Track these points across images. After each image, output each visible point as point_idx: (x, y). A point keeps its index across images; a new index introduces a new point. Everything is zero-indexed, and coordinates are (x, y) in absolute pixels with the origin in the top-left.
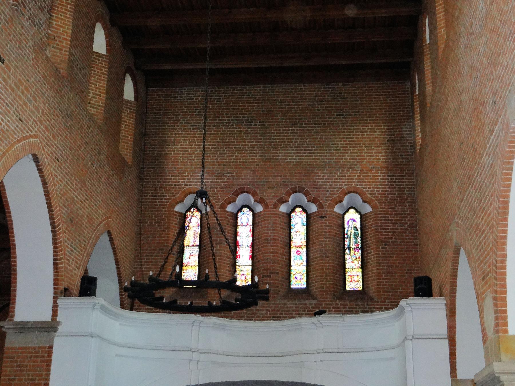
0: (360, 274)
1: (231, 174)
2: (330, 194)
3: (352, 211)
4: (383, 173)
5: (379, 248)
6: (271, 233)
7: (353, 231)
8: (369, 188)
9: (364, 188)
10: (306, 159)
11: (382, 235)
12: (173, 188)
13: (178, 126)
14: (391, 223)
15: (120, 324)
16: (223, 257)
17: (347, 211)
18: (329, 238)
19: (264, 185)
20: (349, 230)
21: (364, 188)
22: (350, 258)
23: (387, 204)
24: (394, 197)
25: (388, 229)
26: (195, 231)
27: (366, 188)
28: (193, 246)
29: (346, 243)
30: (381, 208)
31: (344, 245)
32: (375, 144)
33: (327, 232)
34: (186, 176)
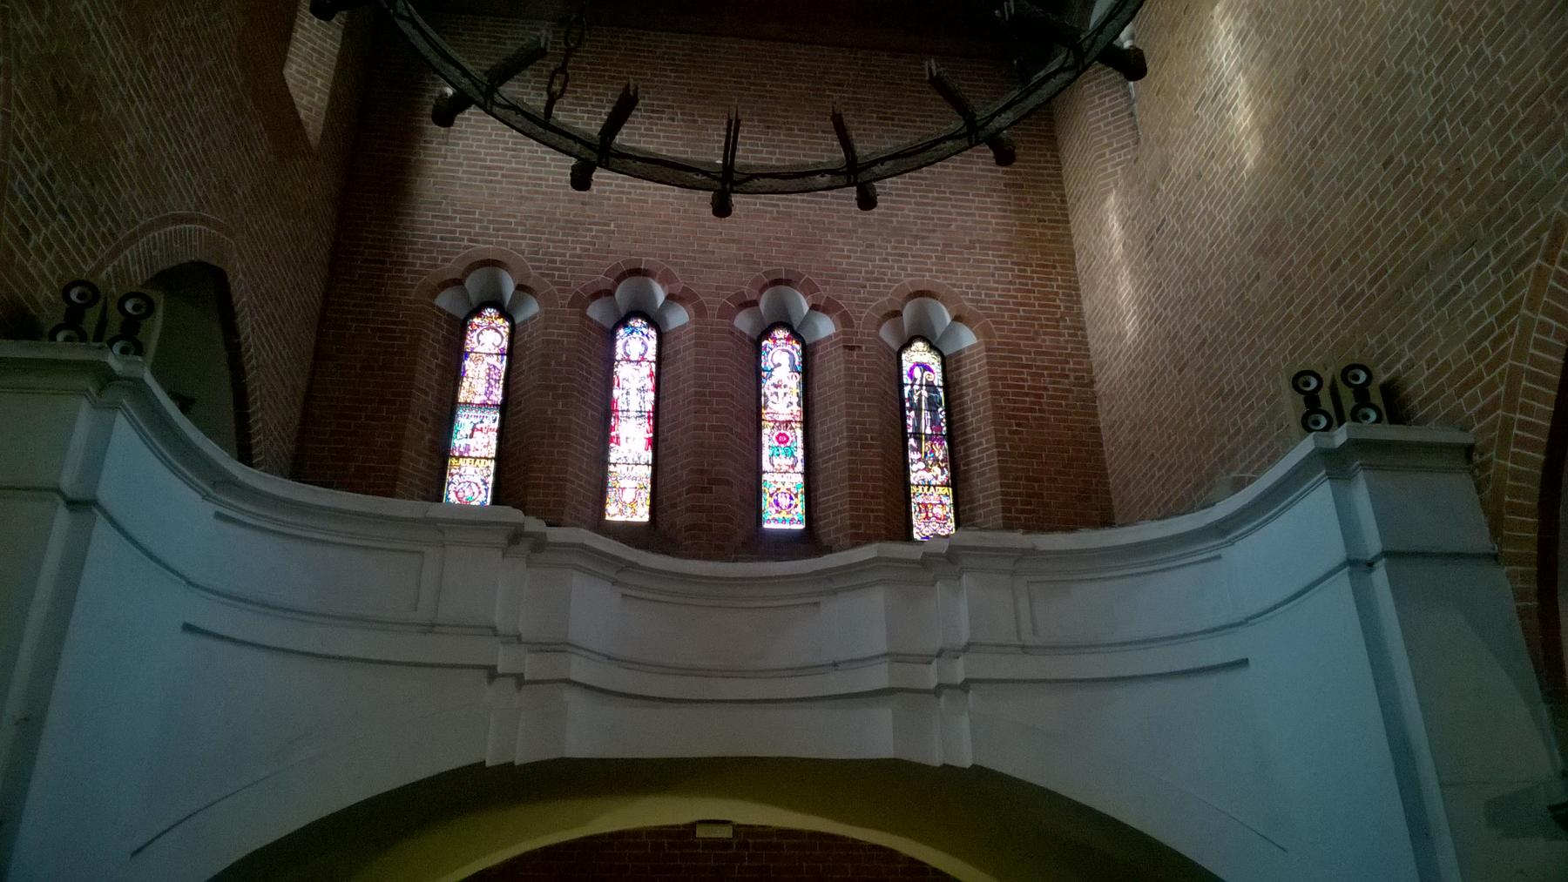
0: (949, 501)
1: (605, 224)
3: (919, 345)
5: (1003, 432)
7: (925, 393)
8: (967, 287)
15: (218, 516)
20: (915, 390)
22: (919, 460)
24: (1030, 312)
25: (1023, 387)
26: (492, 367)
27: (961, 286)
29: (910, 422)
31: (904, 426)
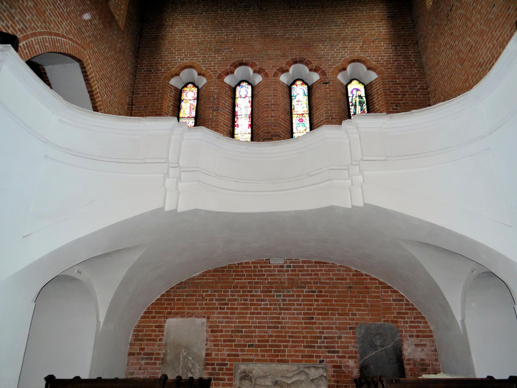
2: (333, 62)
3: (355, 82)
4: (386, 44)
5: (390, 109)
6: (272, 99)
7: (358, 100)
9: (367, 56)
10: (305, 34)
11: (391, 97)
12: (169, 63)
13: (177, 13)
14: (400, 87)
16: (221, 122)
17: (350, 82)
18: (335, 101)
19: (263, 57)
20: (353, 98)
21: (367, 56)
23: (393, 70)
25: (398, 92)
28: (189, 117)
29: (351, 110)
30: (387, 74)
32: (376, 20)
33: (332, 96)
34: (183, 53)
